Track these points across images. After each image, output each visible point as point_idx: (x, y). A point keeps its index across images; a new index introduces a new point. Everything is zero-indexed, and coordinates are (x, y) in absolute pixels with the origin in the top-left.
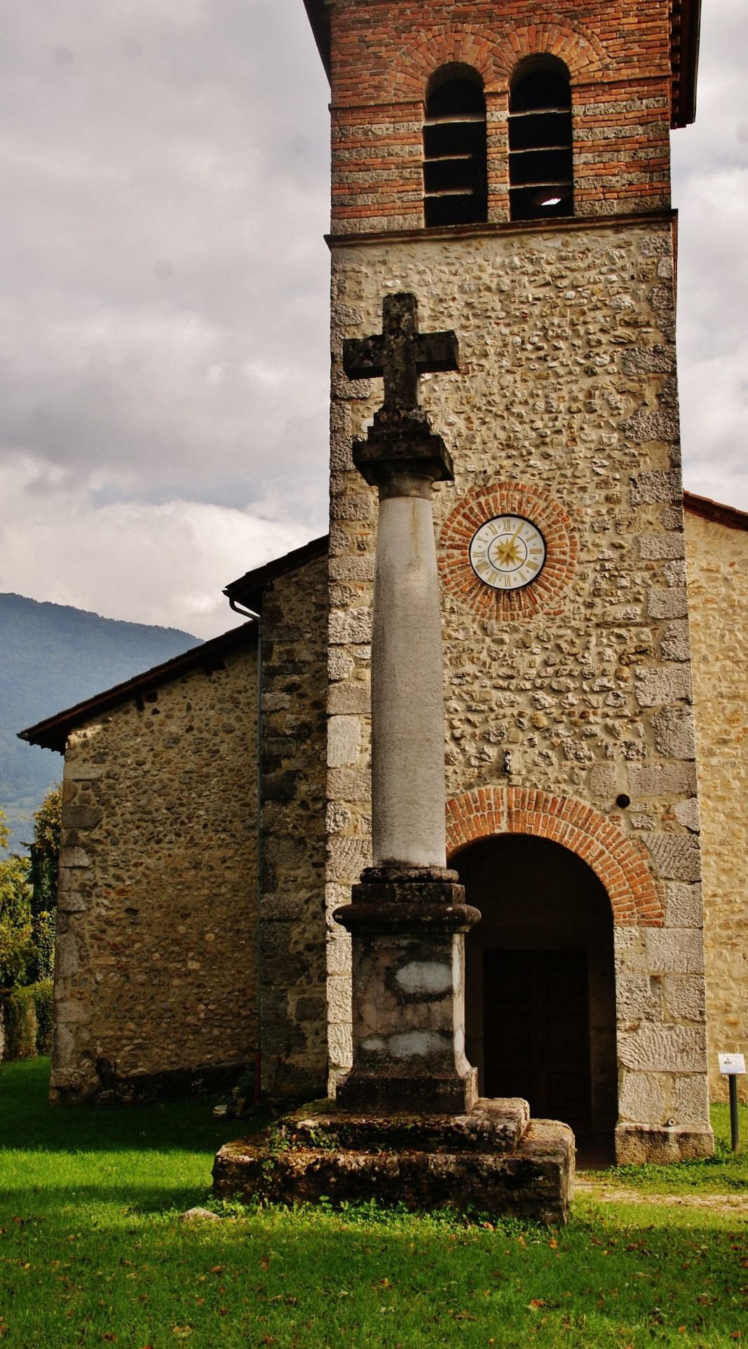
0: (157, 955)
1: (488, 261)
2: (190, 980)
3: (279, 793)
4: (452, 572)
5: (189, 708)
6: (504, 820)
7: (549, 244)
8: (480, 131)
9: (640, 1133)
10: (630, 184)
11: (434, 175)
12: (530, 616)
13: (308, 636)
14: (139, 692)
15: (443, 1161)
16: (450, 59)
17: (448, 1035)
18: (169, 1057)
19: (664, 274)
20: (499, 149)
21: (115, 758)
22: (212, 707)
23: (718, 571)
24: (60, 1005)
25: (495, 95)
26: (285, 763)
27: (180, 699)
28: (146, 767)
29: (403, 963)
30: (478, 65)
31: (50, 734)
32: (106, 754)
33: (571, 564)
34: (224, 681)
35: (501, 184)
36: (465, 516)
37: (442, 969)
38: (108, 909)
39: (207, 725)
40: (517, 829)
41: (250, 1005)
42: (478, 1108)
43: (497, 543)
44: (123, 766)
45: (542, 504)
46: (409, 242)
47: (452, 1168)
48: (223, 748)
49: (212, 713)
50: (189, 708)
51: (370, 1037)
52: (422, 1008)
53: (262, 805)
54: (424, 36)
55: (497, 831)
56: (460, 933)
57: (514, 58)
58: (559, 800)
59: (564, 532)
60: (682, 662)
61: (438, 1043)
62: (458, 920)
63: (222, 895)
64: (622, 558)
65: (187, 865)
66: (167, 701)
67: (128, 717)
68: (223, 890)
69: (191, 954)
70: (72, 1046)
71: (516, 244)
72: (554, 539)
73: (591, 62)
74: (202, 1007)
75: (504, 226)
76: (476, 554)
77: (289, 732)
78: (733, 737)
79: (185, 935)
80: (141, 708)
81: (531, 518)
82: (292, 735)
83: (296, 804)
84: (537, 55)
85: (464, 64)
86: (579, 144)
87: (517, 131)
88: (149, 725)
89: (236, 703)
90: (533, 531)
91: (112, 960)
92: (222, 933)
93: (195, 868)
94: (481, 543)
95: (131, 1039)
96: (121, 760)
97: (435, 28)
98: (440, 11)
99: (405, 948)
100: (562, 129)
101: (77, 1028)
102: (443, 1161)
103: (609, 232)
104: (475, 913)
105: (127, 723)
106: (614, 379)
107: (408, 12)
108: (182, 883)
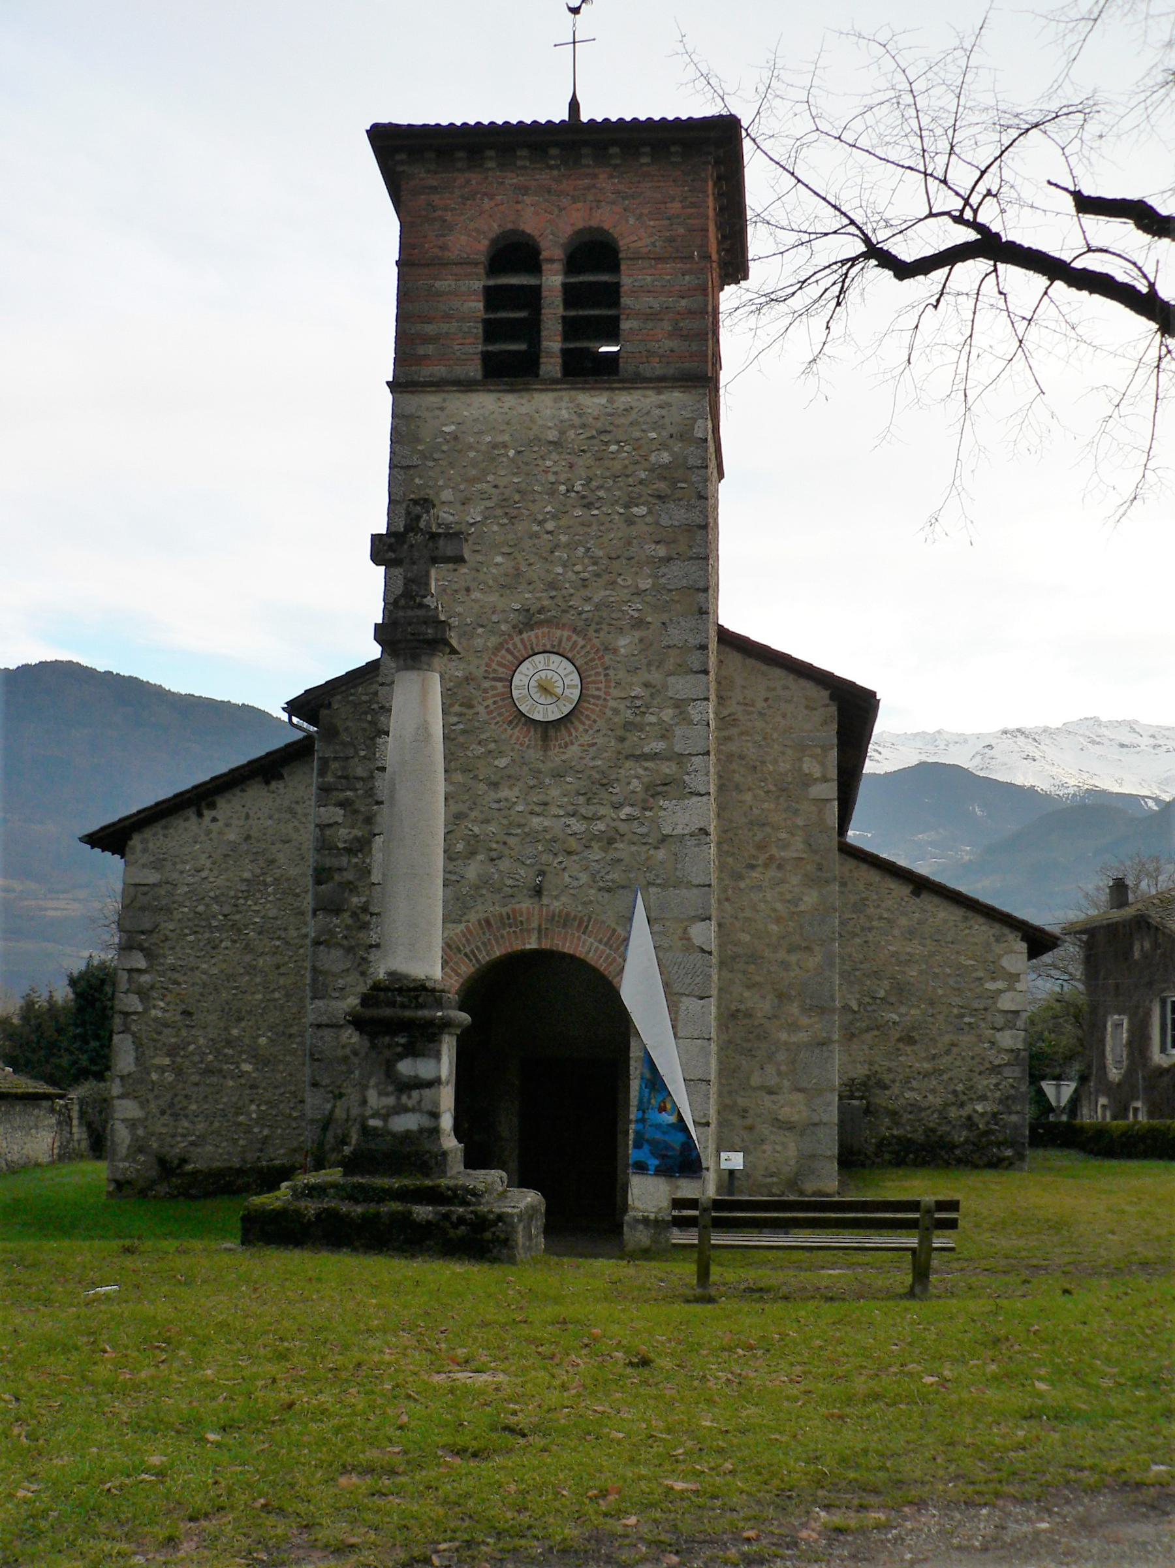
0: (211, 1057)
1: (547, 409)
2: (243, 1081)
3: (329, 907)
4: (495, 703)
5: (247, 817)
6: (534, 936)
7: (596, 400)
8: (536, 291)
9: (646, 1221)
10: (672, 351)
11: (492, 330)
12: (566, 747)
13: (362, 753)
14: (199, 799)
15: (423, 1212)
16: (510, 226)
17: (435, 1115)
18: (221, 1155)
19: (700, 435)
20: (553, 311)
21: (174, 864)
22: (270, 817)
23: (753, 706)
24: (117, 1102)
25: (551, 261)
26: (337, 877)
27: (238, 807)
28: (204, 874)
29: (401, 1057)
30: (536, 233)
31: (112, 839)
32: (164, 860)
33: (605, 700)
34: (282, 791)
35: (553, 343)
36: (508, 650)
37: (432, 1063)
38: (164, 1010)
39: (265, 834)
40: (546, 945)
41: (300, 1107)
42: (457, 1174)
43: (536, 677)
44: (182, 872)
45: (581, 642)
46: (466, 391)
47: (430, 1217)
48: (281, 858)
49: (270, 822)
50: (247, 817)
51: (373, 1116)
52: (415, 1094)
53: (314, 914)
54: (487, 204)
55: (528, 947)
56: (450, 1034)
57: (569, 231)
58: (586, 919)
59: (600, 670)
60: (702, 795)
61: (426, 1122)
62: (446, 1024)
63: (275, 1000)
64: (652, 695)
65: (242, 971)
66: (227, 808)
67: (187, 824)
68: (277, 995)
69: (244, 1057)
70: (128, 1141)
71: (566, 399)
72: (590, 676)
73: (640, 239)
74: (253, 1107)
75: (555, 381)
76: (518, 688)
77: (341, 845)
78: (760, 862)
79: (238, 1038)
80: (200, 815)
81: (570, 655)
82: (344, 848)
83: (346, 915)
84: (590, 228)
85: (523, 232)
86: (628, 311)
87: (571, 295)
88: (208, 833)
89: (294, 814)
90: (571, 668)
91: (167, 1061)
92: (274, 1037)
93: (249, 973)
94: (522, 677)
95: (184, 1136)
96: (179, 867)
97: (499, 197)
98: (502, 183)
99: (402, 1045)
100: (611, 294)
101: (132, 1124)
102: (423, 1212)
103: (650, 393)
104: (465, 1017)
105: (186, 829)
106: (650, 529)
107: (474, 182)
108: (236, 988)
